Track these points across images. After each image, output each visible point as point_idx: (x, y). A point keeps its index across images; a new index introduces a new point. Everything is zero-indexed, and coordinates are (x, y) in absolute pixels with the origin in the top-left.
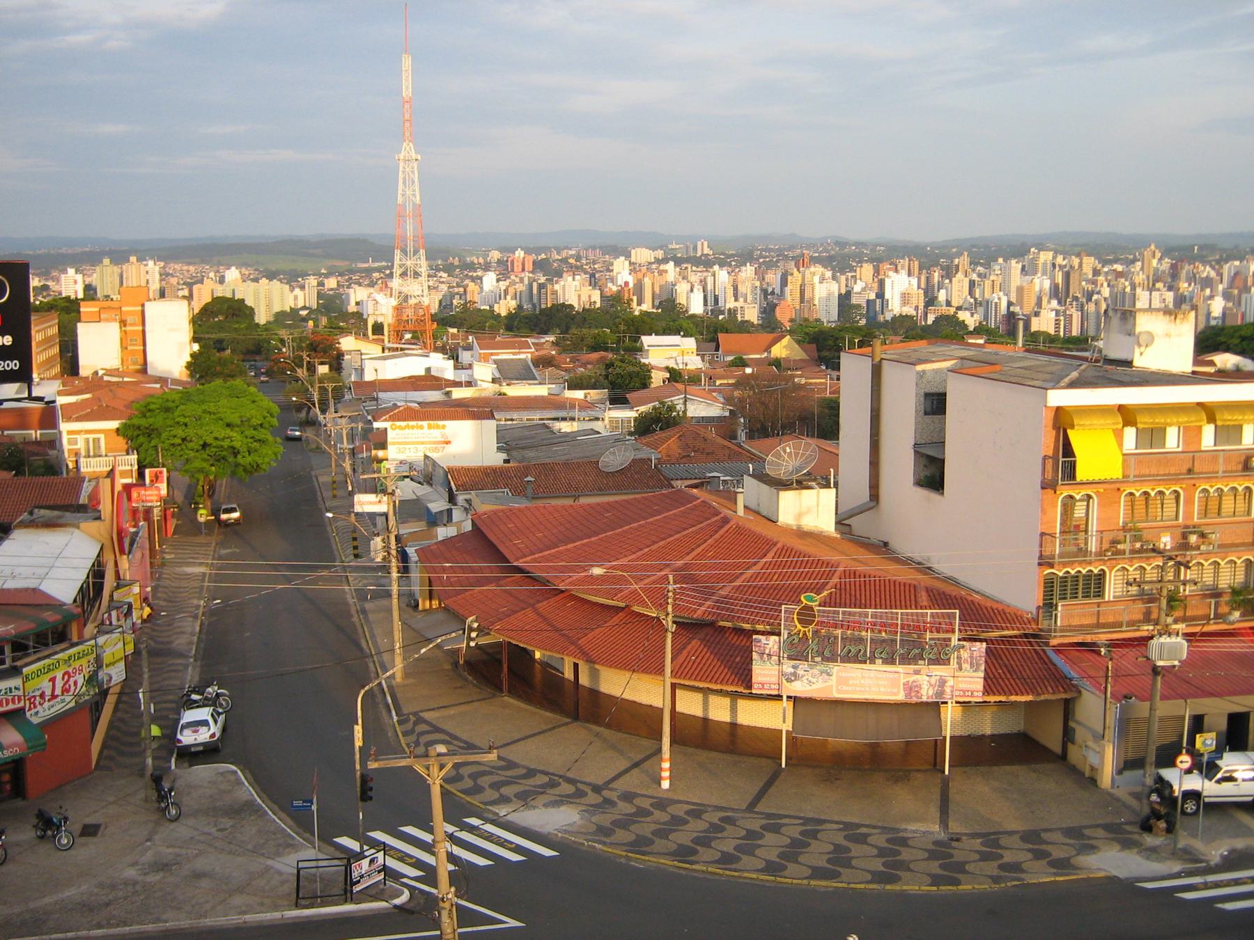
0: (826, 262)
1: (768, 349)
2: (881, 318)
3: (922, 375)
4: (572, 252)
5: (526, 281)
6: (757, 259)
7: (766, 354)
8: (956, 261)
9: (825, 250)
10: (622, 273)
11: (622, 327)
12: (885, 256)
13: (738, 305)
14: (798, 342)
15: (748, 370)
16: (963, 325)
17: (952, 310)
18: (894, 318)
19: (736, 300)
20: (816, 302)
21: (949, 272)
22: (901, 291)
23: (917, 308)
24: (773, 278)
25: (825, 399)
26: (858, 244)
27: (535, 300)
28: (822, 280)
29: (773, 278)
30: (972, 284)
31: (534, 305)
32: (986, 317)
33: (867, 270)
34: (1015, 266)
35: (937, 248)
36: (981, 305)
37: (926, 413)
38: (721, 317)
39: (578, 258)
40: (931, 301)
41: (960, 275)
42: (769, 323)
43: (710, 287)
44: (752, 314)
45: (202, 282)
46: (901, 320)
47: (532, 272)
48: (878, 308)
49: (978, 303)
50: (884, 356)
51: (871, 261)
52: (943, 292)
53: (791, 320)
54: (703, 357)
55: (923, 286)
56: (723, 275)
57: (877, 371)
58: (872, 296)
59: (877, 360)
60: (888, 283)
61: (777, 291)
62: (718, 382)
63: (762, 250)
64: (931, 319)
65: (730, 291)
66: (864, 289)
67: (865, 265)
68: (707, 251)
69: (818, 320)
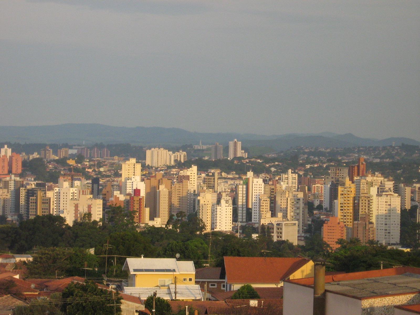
0: (386, 170)
4: (71, 152)
5: (12, 186)
6: (303, 165)
10: (132, 178)
11: (107, 246)
13: (274, 221)
20: (374, 220)
24: (321, 188)
27: (22, 211)
29: (321, 188)
31: (20, 216)
39: (80, 159)
43: (241, 201)
44: (291, 234)
47: (21, 176)
50: (329, 287)
53: (340, 242)
54: (202, 285)
56: (258, 185)
59: (320, 292)
63: (310, 153)
65: (266, 205)
68: (240, 153)
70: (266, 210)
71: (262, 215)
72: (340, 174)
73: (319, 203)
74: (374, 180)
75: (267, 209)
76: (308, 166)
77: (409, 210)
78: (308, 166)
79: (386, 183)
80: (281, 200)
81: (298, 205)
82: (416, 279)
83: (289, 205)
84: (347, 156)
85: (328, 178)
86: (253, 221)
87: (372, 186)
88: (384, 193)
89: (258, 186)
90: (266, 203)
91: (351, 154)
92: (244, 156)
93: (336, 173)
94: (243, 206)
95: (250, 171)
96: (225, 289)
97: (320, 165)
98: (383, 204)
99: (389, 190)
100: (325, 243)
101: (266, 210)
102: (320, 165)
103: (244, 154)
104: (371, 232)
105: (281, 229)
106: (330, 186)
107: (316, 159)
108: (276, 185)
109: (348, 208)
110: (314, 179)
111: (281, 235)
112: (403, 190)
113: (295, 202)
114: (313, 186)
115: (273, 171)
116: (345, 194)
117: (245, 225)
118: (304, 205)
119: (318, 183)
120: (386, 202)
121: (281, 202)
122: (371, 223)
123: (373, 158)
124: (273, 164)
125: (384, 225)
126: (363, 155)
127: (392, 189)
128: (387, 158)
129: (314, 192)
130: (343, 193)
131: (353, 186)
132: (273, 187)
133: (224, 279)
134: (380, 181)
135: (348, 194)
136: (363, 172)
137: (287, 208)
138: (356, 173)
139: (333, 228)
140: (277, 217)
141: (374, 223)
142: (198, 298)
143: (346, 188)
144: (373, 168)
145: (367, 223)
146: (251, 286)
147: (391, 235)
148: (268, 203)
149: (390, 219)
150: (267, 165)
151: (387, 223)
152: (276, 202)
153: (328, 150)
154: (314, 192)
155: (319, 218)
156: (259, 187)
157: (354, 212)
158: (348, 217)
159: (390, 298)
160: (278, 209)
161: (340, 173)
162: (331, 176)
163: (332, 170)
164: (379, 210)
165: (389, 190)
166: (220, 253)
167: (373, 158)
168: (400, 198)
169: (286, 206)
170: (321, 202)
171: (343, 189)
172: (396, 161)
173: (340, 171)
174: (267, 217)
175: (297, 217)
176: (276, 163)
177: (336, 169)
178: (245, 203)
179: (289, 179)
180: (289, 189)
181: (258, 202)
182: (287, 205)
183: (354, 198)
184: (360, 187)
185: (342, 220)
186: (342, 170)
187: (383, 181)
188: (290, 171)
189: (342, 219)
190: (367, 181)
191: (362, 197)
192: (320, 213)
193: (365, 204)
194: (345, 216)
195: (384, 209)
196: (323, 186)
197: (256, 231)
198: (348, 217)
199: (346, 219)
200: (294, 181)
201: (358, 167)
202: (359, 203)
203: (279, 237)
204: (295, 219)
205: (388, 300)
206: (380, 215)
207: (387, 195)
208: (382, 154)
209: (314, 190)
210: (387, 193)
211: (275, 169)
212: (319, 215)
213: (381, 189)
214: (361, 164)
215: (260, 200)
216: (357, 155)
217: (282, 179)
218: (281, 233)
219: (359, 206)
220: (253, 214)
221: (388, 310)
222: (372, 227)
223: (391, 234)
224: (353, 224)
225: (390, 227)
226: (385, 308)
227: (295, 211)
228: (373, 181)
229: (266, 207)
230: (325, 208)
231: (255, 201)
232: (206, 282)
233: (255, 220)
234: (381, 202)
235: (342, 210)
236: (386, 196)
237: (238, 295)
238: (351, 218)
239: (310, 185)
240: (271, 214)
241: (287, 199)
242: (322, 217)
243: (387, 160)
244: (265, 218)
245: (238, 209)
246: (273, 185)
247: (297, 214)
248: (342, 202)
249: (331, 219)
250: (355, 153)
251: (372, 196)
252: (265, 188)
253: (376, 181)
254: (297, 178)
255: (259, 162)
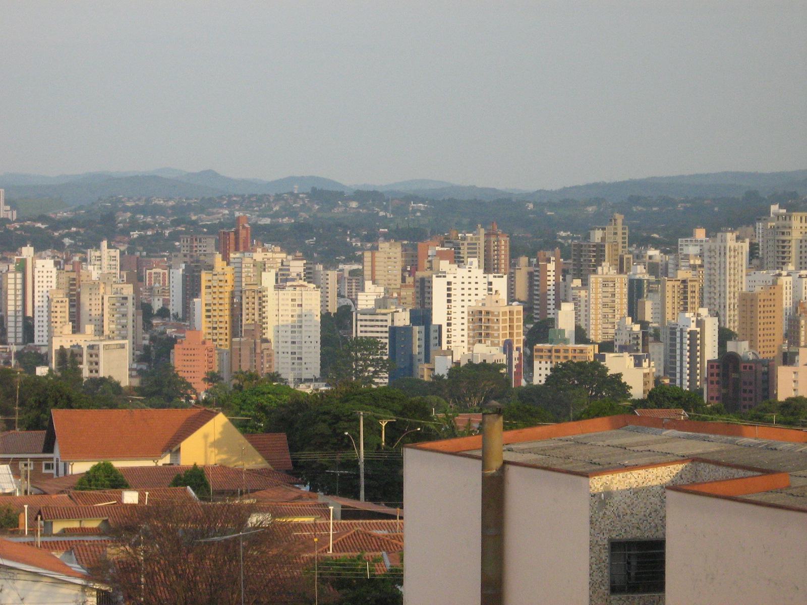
1: (172, 446)
2: (424, 373)
3: (603, 500)
6: (125, 232)
7: (167, 459)
8: (597, 236)
9: (293, 214)
12: (430, 224)
14: (244, 427)
15: (130, 497)
16: (617, 384)
17: (591, 351)
18: (456, 371)
19: (77, 329)
20: (270, 334)
21: (581, 262)
22: (468, 307)
23: (508, 347)
25: (325, 563)
26: (362, 196)
28: (282, 280)
30: (636, 290)
32: (670, 368)
33: (388, 258)
34: (735, 246)
35: (552, 205)
36: (657, 337)
37: (614, 590)
38: (42, 371)
40: (540, 330)
41: (607, 269)
42: (158, 382)
44: (116, 364)
45: (373, 284)
46: (473, 380)
48: (417, 348)
49: (649, 336)
50: (508, 456)
51: (395, 235)
52: (567, 308)
55: (522, 292)
57: (494, 493)
58: (403, 319)
59: (495, 465)
60: (438, 287)
61: (176, 307)
62: (57, 527)
63: (136, 210)
64: (541, 372)
65: (63, 311)
66: (381, 303)
67: (384, 246)
69: (274, 377)
70: (63, 320)
71: (55, 330)
72: (200, 249)
73: (161, 305)
74: (268, 259)
75: (64, 317)
76: (135, 234)
77: (335, 314)
78: (135, 234)
79: (293, 263)
80: (90, 299)
81: (123, 309)
82: (654, 437)
83: (106, 310)
84: (209, 214)
85: (176, 256)
86: (36, 343)
87: (264, 270)
88: (289, 284)
89: (45, 274)
90: (61, 307)
91: (215, 210)
92: (10, 217)
93: (192, 247)
94: (16, 314)
95: (28, 245)
96: (54, 471)
97: (157, 231)
98: (287, 305)
99: (298, 278)
100: (183, 381)
101: (63, 320)
102: (157, 231)
103: (10, 213)
104: (265, 358)
105: (97, 355)
106: (183, 270)
107: (149, 219)
108: (79, 271)
109: (221, 313)
110: (148, 259)
111: (96, 367)
112: (322, 277)
113: (118, 304)
114: (148, 271)
115: (67, 244)
116: (215, 287)
117: (22, 350)
118: (134, 309)
119: (158, 266)
120: (292, 300)
121: (90, 305)
122: (266, 341)
123: (258, 216)
124: (67, 231)
125: (289, 344)
126: (238, 210)
127: (302, 275)
128: (283, 217)
129: (150, 284)
130: (209, 284)
131: (229, 270)
132: (74, 275)
133: (52, 451)
134: (280, 261)
135: (221, 287)
136: (245, 242)
137: (103, 315)
138: (232, 246)
139: (192, 352)
140: (84, 333)
141: (272, 341)
142: (7, 491)
143: (216, 275)
144: (268, 235)
145: (258, 341)
146: (112, 466)
147: (303, 363)
148: (65, 307)
149: (301, 332)
150: (56, 234)
151: (296, 340)
152: (81, 306)
153: (171, 203)
154: (150, 284)
155: (164, 333)
156: (47, 277)
157: (233, 321)
158: (221, 331)
159: (640, 471)
160: (84, 317)
161: (200, 246)
162: (182, 252)
163: (184, 241)
164: (280, 315)
165: (298, 278)
166: (33, 403)
167: (258, 216)
168: (319, 293)
169: (100, 312)
170: (166, 302)
171: (210, 277)
172: (301, 220)
173: (200, 241)
174: (64, 333)
175: (122, 332)
176: (74, 229)
177: (192, 239)
178: (20, 308)
179: (103, 260)
180: (105, 279)
181: (45, 304)
182: (103, 310)
183: (232, 293)
184: (241, 272)
185: (210, 337)
186: (203, 240)
187: (285, 260)
188: (104, 244)
189: (209, 334)
190: (255, 260)
191: (247, 292)
192: (164, 324)
193: (253, 305)
194: (215, 328)
195: (290, 313)
196: (166, 271)
197: (43, 360)
198: (221, 331)
199: (216, 334)
200: (114, 263)
201: (237, 233)
202: (241, 304)
203: (94, 371)
204: (118, 335)
205: (636, 476)
206: (283, 326)
207: (295, 287)
208: (275, 209)
209: (150, 280)
210: (294, 283)
211: (71, 241)
212: (162, 328)
213: (283, 275)
214: (241, 227)
215: (49, 300)
216: (227, 212)
217: (89, 260)
218: (97, 364)
219: (241, 309)
220: (36, 329)
221: (636, 495)
222: (268, 349)
223: (303, 361)
224: (231, 343)
225: (301, 348)
226: (632, 490)
227: (118, 321)
228: (265, 260)
229: (63, 315)
230: (173, 314)
231: (40, 304)
232: (27, 458)
233: (41, 339)
234: (283, 299)
235: (209, 317)
236: (292, 288)
237: (87, 483)
238: (227, 331)
239: (142, 269)
240: (72, 328)
241: (103, 298)
242: (168, 331)
243: (285, 220)
244: (61, 335)
245: (7, 318)
246: (73, 271)
247: (123, 327)
248: (208, 302)
249: (188, 334)
250: (222, 207)
251: (266, 289)
252: (58, 277)
253: (271, 260)
254: (118, 258)
255: (39, 228)
